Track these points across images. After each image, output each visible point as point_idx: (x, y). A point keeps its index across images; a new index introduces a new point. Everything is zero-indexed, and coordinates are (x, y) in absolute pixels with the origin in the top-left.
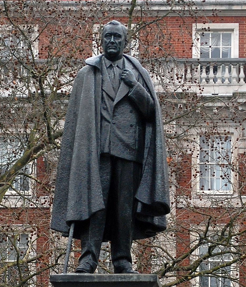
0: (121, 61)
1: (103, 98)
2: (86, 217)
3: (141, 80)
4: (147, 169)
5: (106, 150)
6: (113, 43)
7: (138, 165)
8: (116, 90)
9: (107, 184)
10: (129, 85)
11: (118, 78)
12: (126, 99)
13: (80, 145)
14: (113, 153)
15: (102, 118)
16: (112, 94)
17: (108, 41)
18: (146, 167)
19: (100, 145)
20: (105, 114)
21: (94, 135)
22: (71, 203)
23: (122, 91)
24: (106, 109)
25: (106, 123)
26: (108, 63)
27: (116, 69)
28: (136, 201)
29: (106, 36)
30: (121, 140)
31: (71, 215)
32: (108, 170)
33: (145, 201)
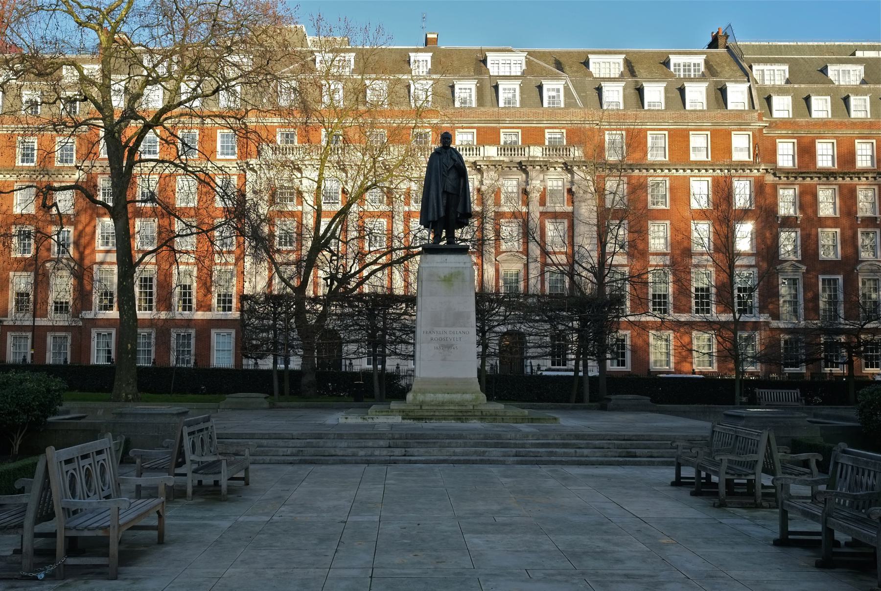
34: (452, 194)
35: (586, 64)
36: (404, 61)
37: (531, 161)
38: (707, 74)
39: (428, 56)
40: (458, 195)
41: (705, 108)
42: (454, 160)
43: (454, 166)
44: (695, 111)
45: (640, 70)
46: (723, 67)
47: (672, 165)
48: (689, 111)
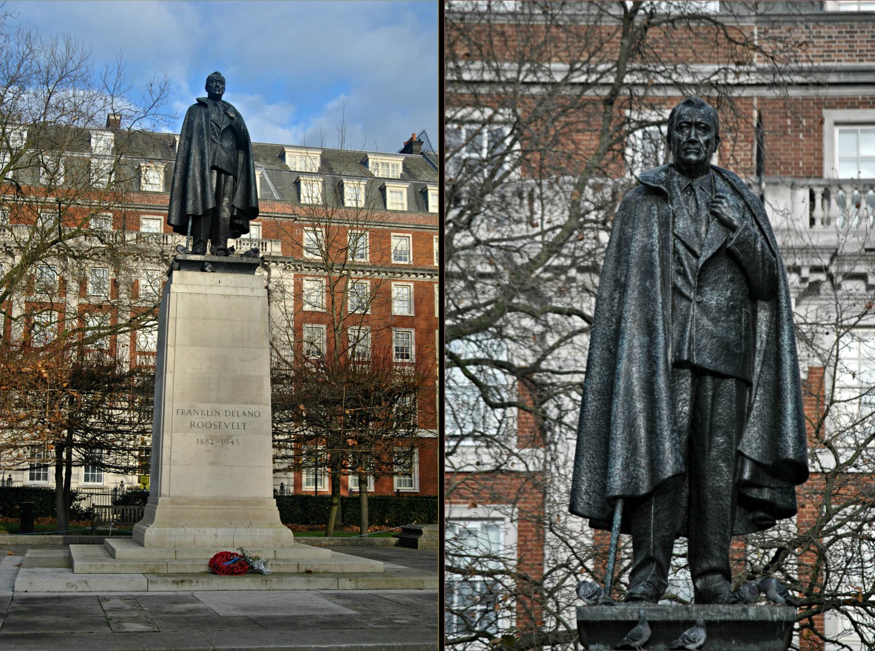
1: (676, 252)
15: (676, 290)
20: (680, 282)
24: (684, 275)
25: (684, 303)
28: (740, 454)
33: (755, 456)
34: (718, 376)
35: (282, 156)
36: (83, 139)
37: (273, 257)
38: (406, 176)
39: (110, 136)
40: (745, 383)
41: (406, 209)
42: (727, 225)
43: (724, 252)
44: (396, 211)
45: (337, 168)
46: (421, 171)
47: (374, 266)
48: (390, 211)
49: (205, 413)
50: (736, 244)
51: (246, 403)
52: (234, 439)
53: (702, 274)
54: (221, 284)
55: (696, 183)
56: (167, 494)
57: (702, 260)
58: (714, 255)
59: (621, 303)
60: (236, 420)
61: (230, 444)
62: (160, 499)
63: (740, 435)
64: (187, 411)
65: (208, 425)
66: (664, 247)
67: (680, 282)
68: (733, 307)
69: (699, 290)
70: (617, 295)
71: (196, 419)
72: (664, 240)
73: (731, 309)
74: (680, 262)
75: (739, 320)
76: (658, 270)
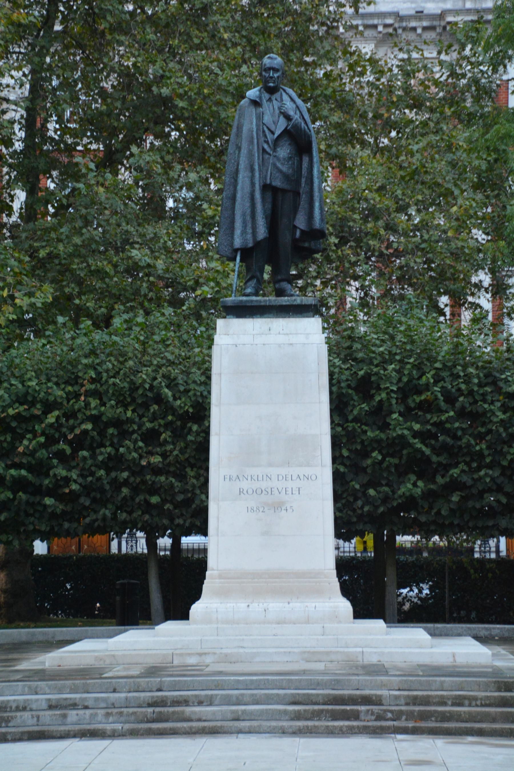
0: (279, 93)
1: (264, 131)
2: (250, 245)
3: (298, 112)
4: (304, 198)
5: (268, 182)
6: (271, 78)
7: (297, 194)
8: (275, 123)
9: (269, 212)
10: (288, 118)
11: (277, 112)
12: (286, 132)
13: (244, 177)
14: (274, 184)
15: (264, 150)
16: (273, 128)
17: (267, 75)
18: (304, 196)
19: (263, 177)
20: (266, 146)
21: (256, 167)
22: (238, 232)
23: (282, 125)
24: (267, 142)
25: (267, 156)
26: (266, 96)
27: (275, 102)
28: (295, 227)
29: (265, 70)
30: (280, 171)
31: (238, 243)
32: (269, 200)
33: (302, 227)
49: (255, 478)
50: (292, 127)
51: (301, 466)
52: (288, 506)
53: (276, 141)
54: (272, 332)
55: (273, 98)
56: (215, 568)
57: (276, 135)
58: (281, 133)
59: (239, 157)
60: (290, 484)
61: (284, 512)
62: (208, 573)
63: (294, 218)
64: (235, 476)
65: (259, 491)
66: (258, 130)
67: (266, 146)
68: (291, 158)
69: (275, 150)
70: (237, 152)
71: (245, 485)
72: (258, 125)
73: (290, 158)
74: (265, 136)
75: (294, 164)
76: (255, 141)
